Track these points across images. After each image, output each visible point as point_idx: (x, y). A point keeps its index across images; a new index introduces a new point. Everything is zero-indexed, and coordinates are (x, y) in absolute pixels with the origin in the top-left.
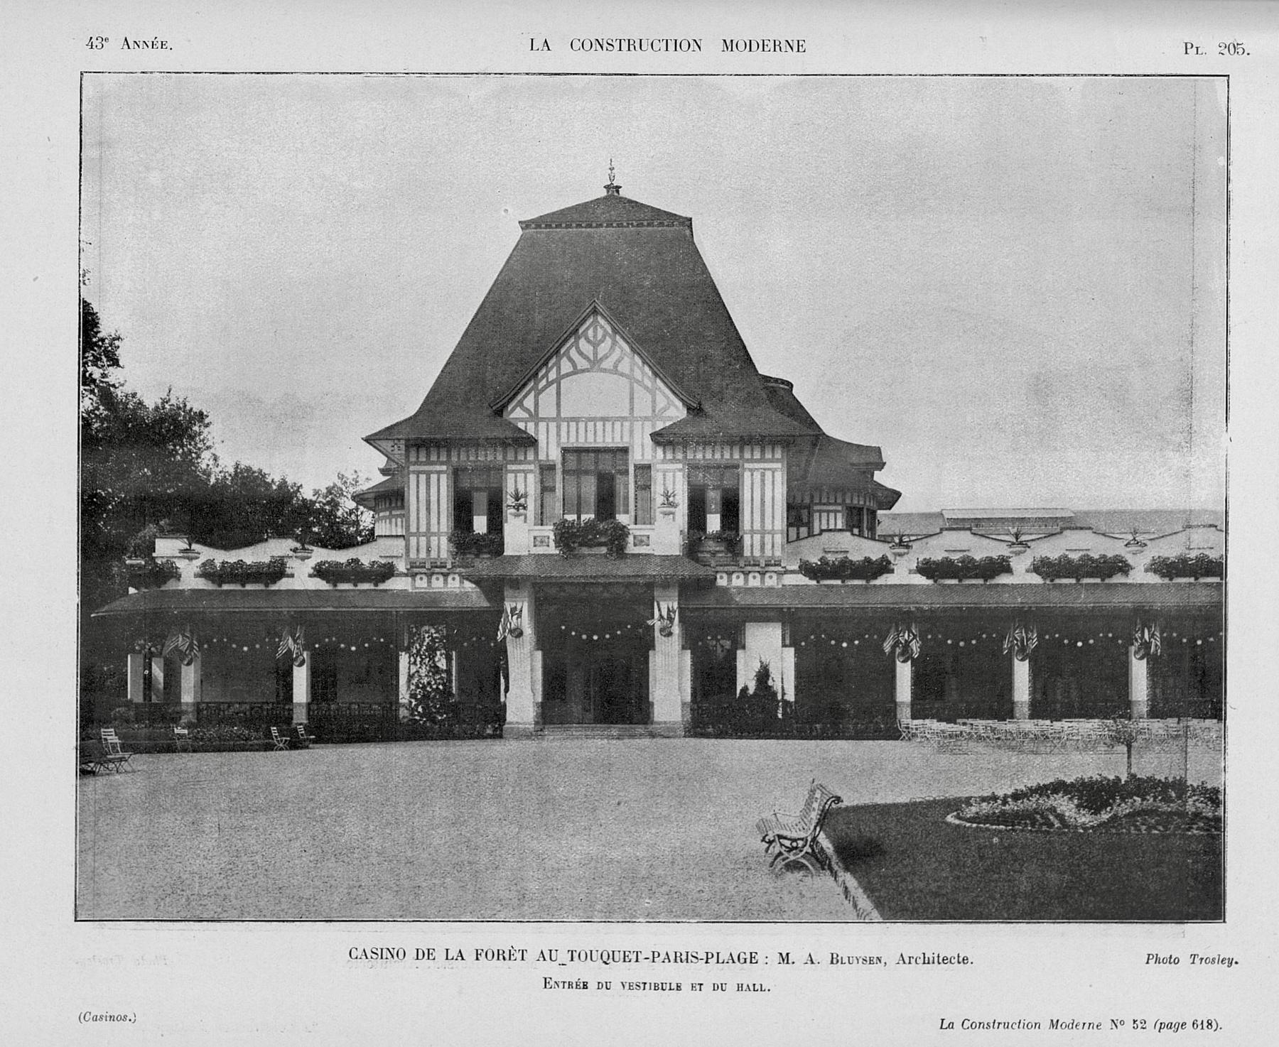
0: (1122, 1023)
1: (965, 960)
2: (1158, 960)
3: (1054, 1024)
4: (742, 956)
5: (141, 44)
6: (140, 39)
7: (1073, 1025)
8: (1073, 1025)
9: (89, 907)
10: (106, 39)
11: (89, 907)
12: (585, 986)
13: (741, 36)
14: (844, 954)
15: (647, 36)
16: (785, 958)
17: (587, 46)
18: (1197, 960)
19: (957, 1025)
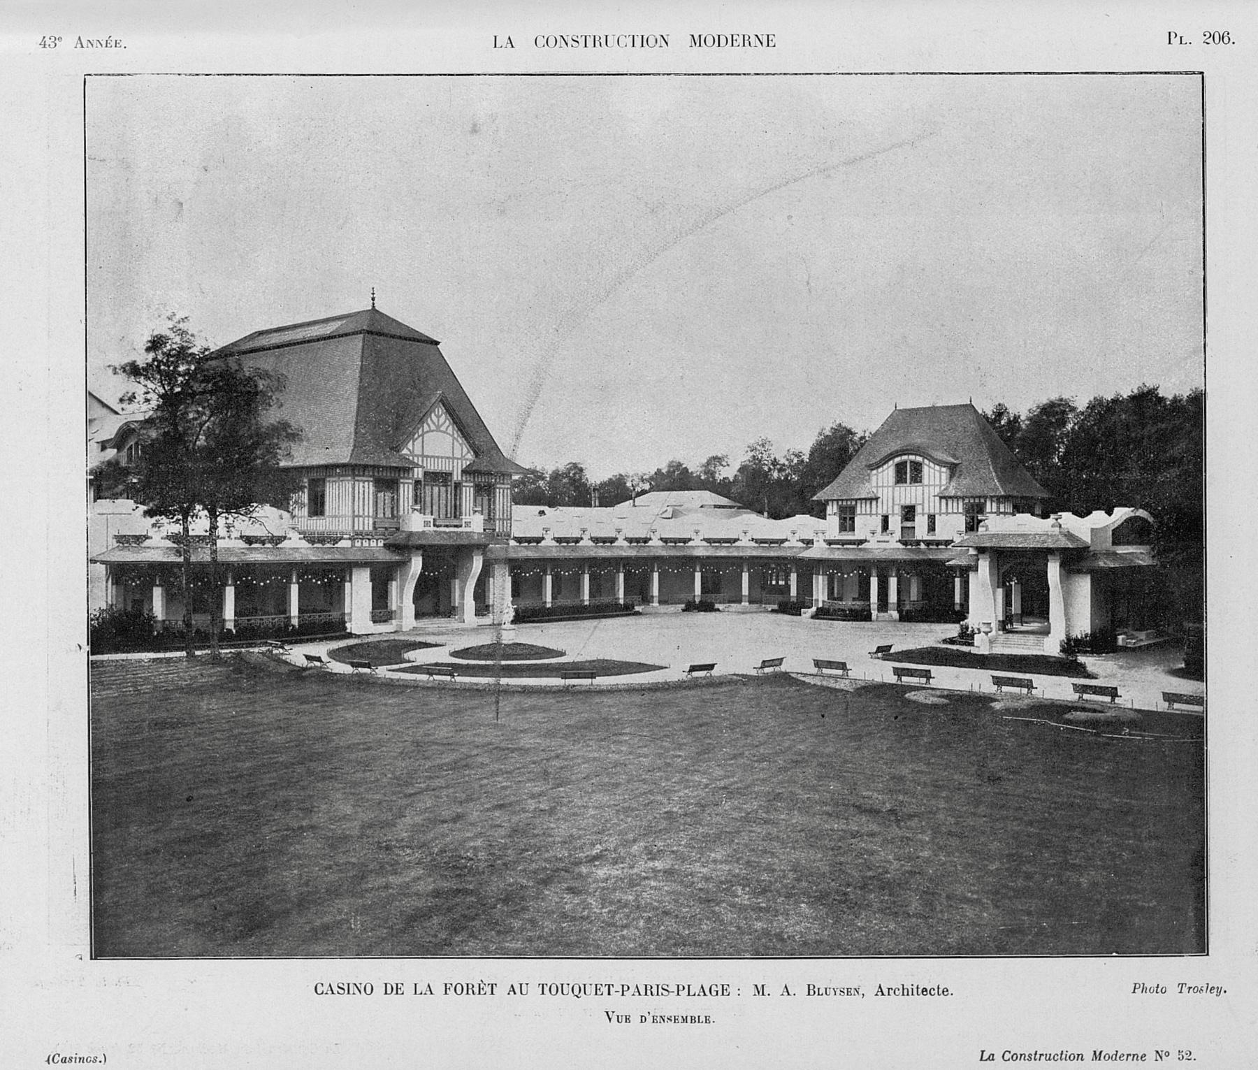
0: (1168, 1054)
1: (945, 991)
2: (1144, 990)
3: (1097, 1056)
4: (714, 988)
5: (95, 43)
6: (93, 38)
7: (1116, 1056)
8: (1116, 1056)
9: (108, 939)
10: (60, 39)
11: (108, 939)
12: (627, 1019)
13: (709, 31)
14: (821, 985)
15: (613, 33)
16: (760, 990)
17: (552, 42)
18: (1185, 989)
19: (998, 1057)
